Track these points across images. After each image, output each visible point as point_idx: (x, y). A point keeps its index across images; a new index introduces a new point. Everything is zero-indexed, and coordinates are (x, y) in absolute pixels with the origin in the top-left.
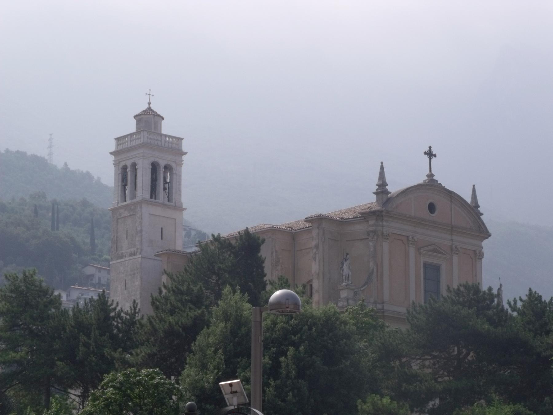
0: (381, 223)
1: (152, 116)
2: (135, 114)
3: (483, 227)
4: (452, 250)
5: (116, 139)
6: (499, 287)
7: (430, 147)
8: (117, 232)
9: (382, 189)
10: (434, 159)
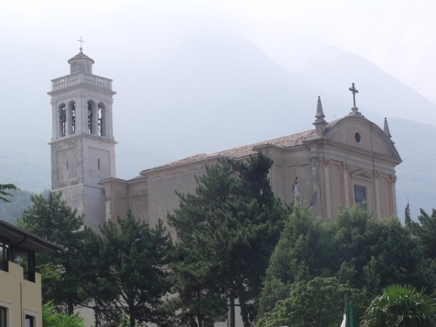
0: (322, 150)
1: (85, 60)
2: (70, 59)
3: (396, 154)
4: (374, 174)
5: (52, 81)
6: (406, 207)
7: (353, 84)
8: (57, 164)
9: (320, 120)
10: (356, 94)
